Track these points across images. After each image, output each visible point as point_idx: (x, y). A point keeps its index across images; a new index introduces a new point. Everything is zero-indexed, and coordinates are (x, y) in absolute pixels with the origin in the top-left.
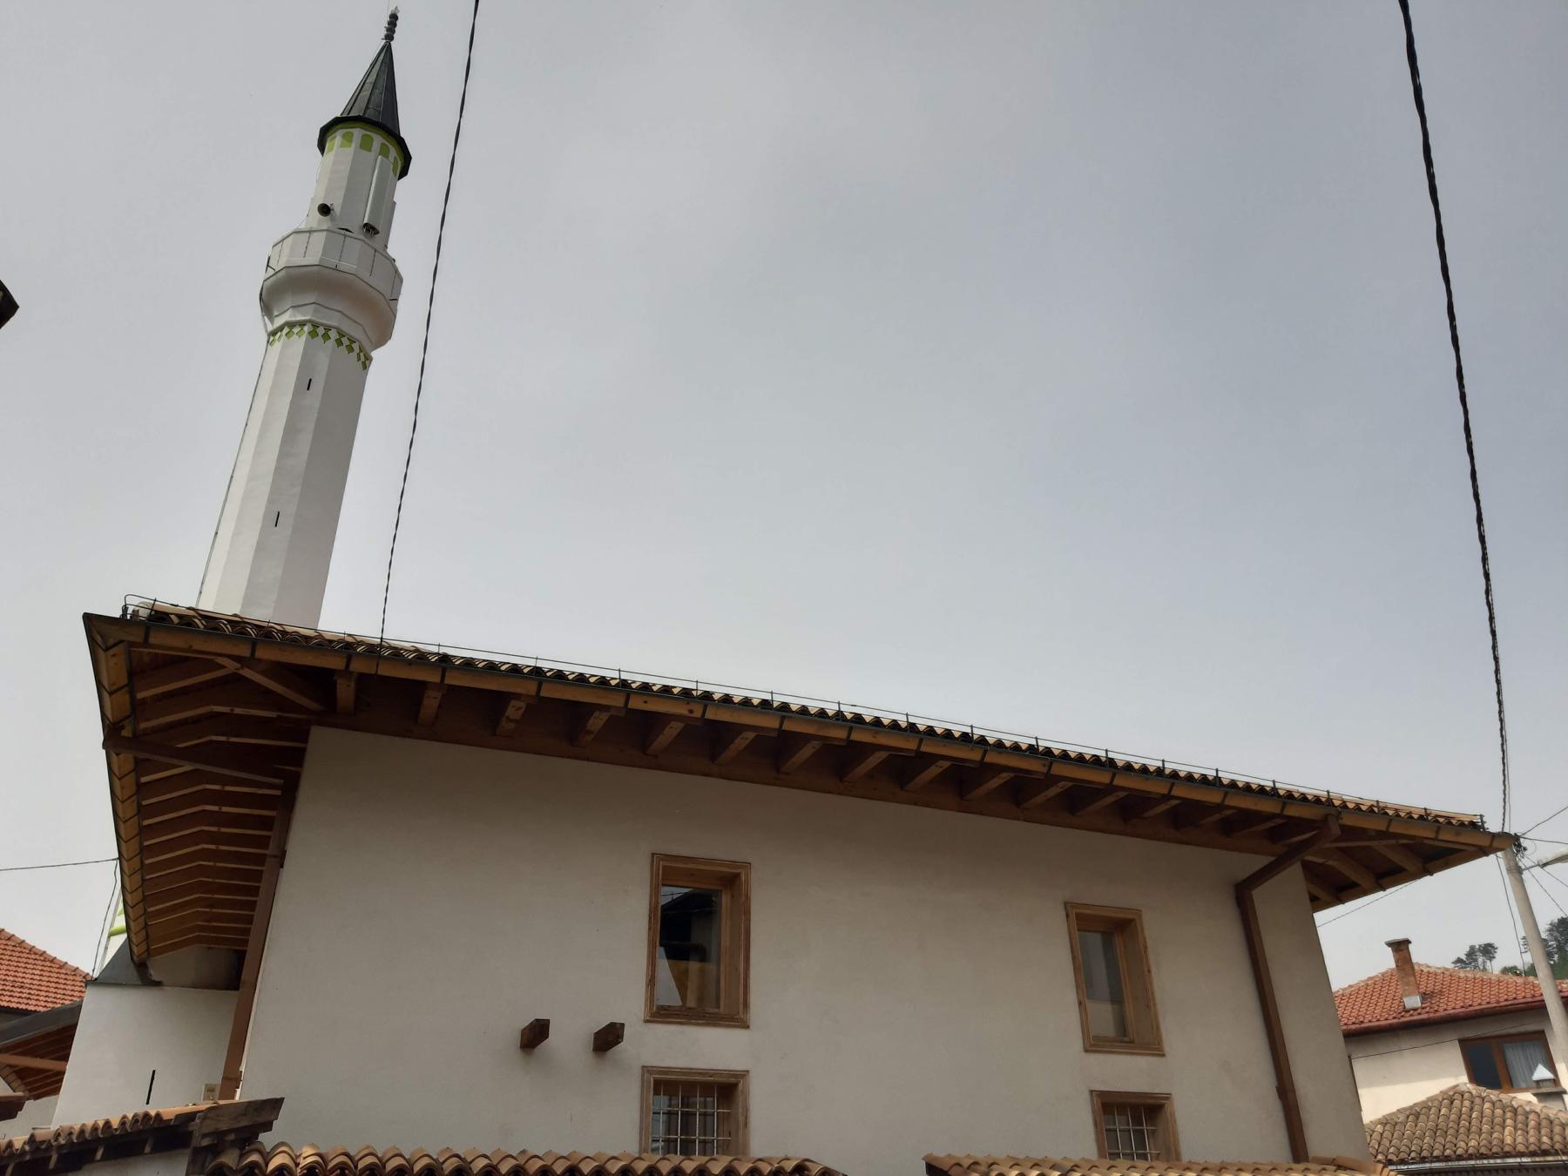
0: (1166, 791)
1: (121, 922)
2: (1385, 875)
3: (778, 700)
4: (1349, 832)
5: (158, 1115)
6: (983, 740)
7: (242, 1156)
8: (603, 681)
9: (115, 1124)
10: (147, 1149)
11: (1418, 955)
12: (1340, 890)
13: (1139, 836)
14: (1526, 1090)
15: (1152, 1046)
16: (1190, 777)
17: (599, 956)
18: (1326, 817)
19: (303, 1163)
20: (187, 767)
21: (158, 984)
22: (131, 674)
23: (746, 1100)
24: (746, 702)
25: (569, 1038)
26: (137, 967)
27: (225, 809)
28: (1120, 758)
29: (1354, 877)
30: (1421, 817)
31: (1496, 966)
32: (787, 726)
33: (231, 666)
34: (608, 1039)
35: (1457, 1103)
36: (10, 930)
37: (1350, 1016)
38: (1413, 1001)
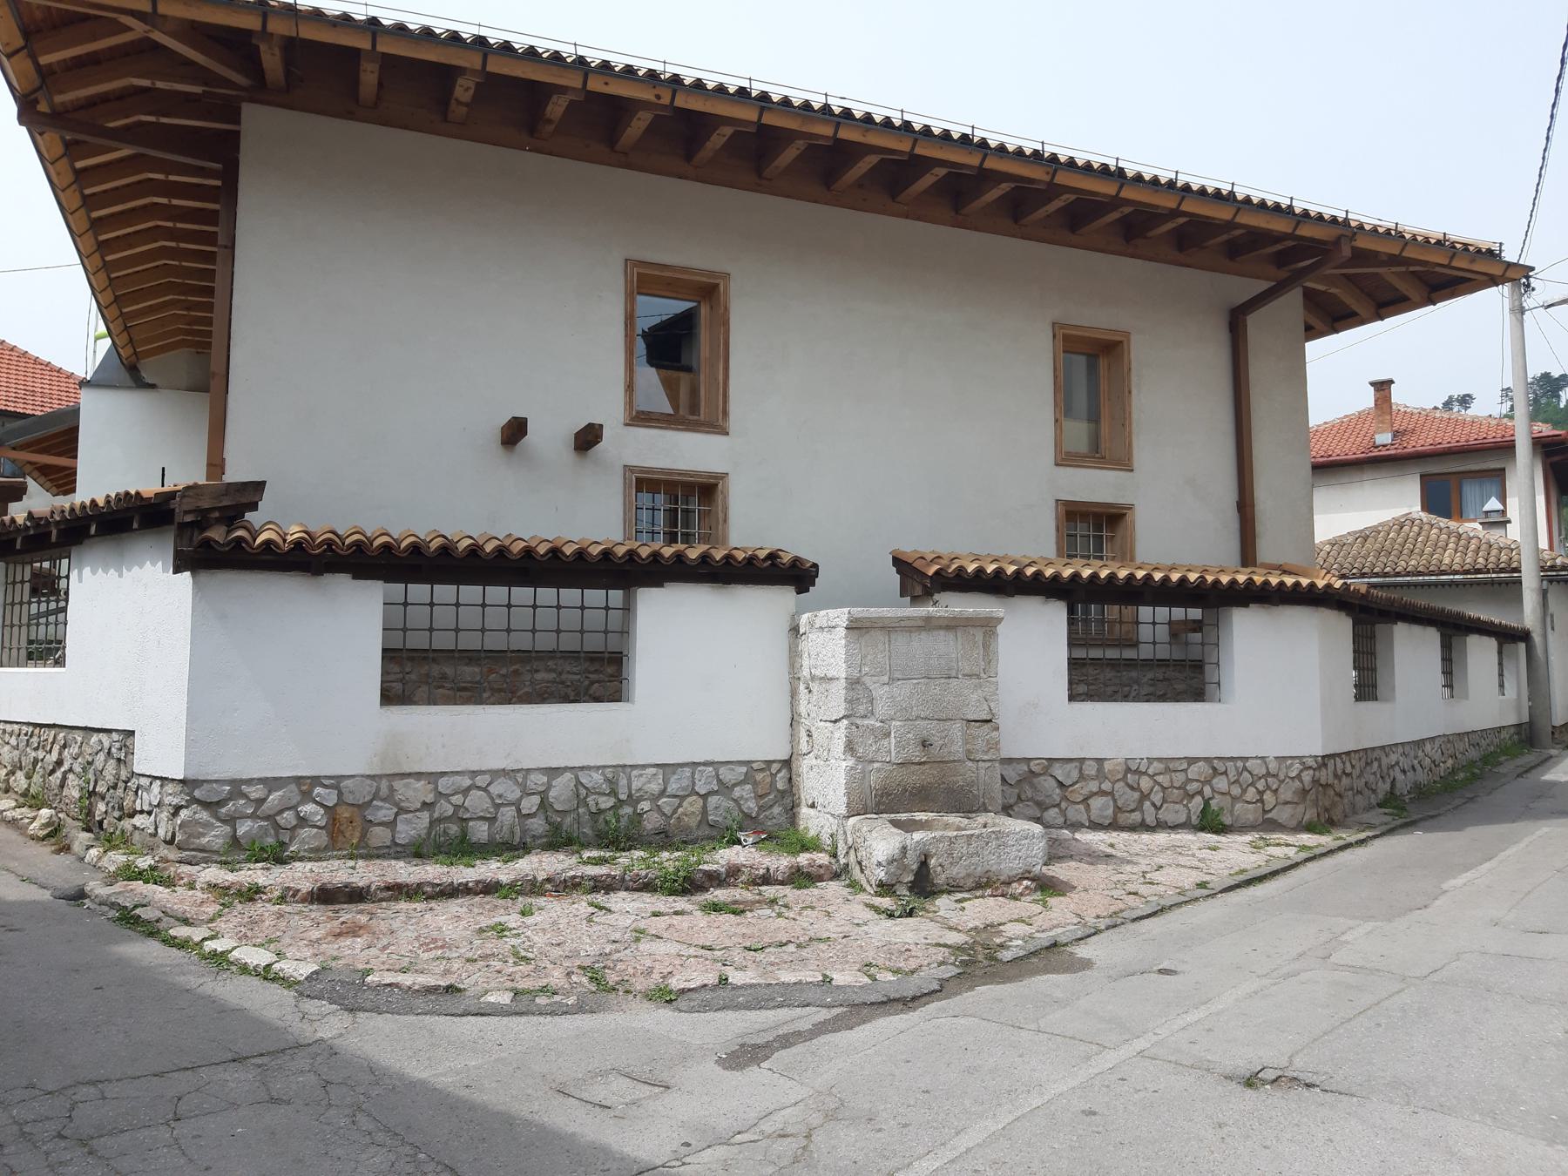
0: (1173, 205)
1: (102, 329)
2: (1386, 303)
3: (756, 88)
4: (1361, 256)
5: (138, 493)
6: (983, 143)
7: (229, 532)
8: (556, 57)
9: (101, 503)
10: (135, 526)
11: (1398, 396)
12: (1333, 316)
13: (1139, 257)
14: (1474, 520)
15: (1123, 463)
16: (1202, 191)
17: (579, 359)
18: (1339, 238)
19: (289, 539)
20: (126, 152)
21: (153, 386)
22: (27, 33)
23: (725, 498)
24: (721, 89)
25: (550, 434)
26: (129, 368)
27: (175, 202)
28: (1131, 169)
29: (1355, 307)
30: (1438, 242)
31: (1476, 410)
32: (768, 119)
33: (139, 29)
34: (587, 439)
35: (1406, 528)
36: (11, 341)
37: (1320, 450)
38: (1384, 438)
